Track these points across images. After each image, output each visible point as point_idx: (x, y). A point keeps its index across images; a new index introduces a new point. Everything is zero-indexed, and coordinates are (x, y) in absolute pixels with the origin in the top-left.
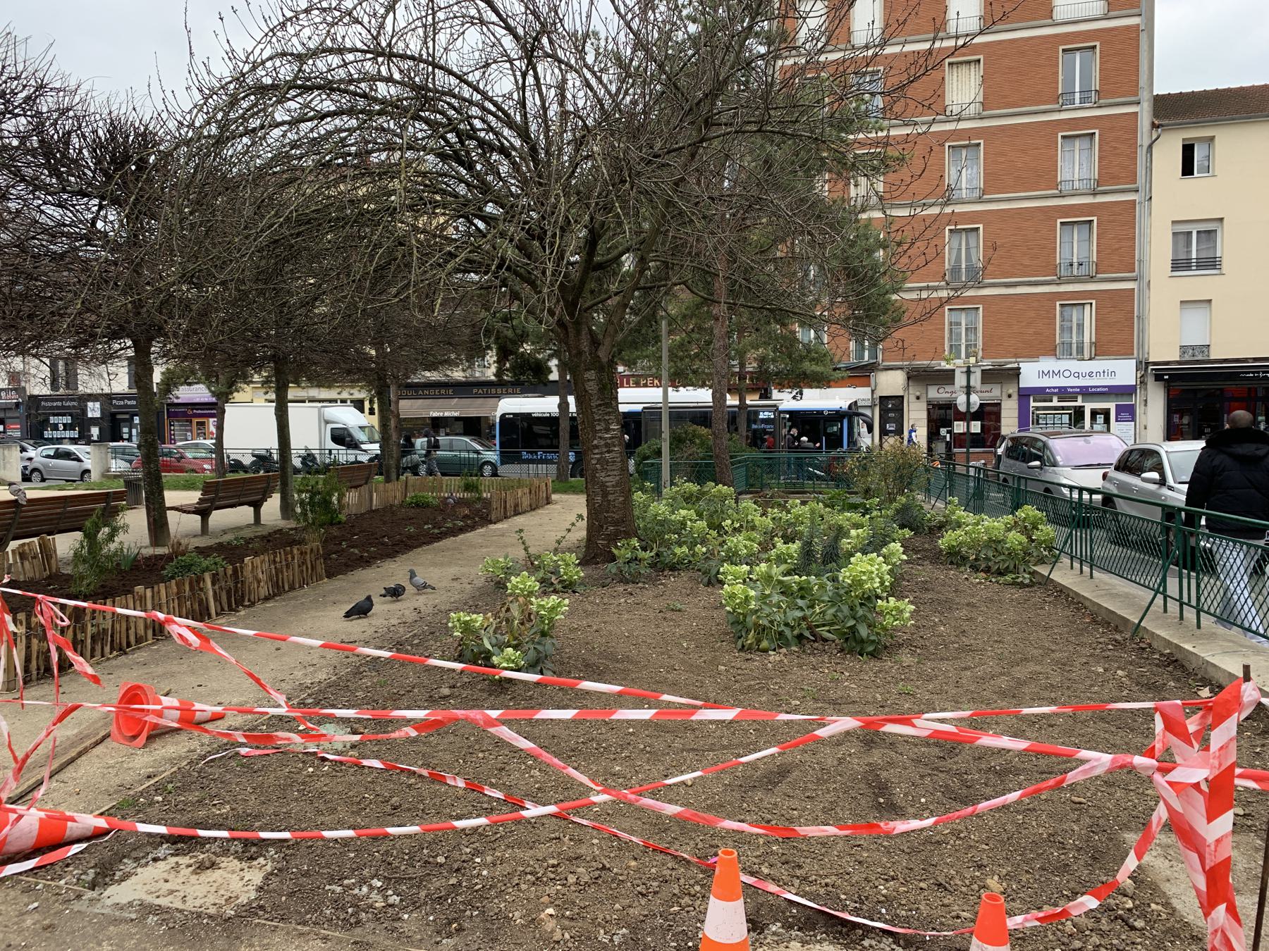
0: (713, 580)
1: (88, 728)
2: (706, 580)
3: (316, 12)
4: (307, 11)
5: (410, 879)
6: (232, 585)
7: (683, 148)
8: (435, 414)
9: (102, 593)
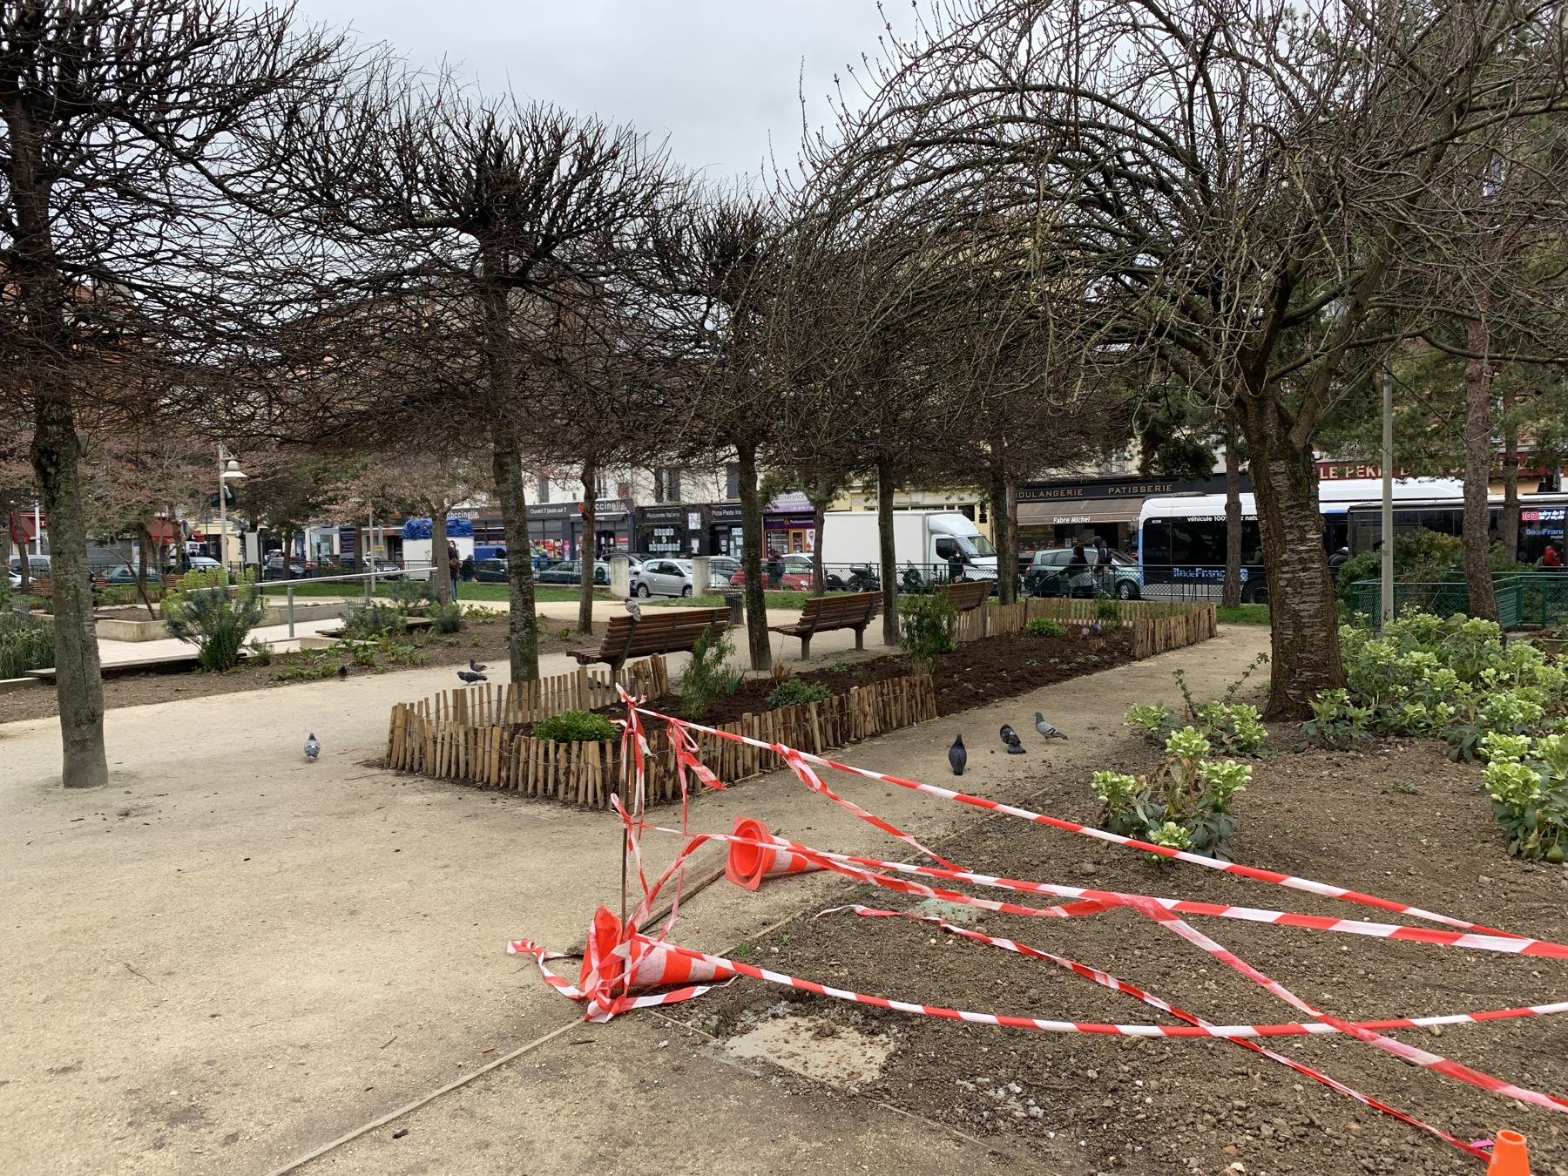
0: (1467, 754)
1: (704, 862)
2: (1455, 752)
3: (938, 54)
4: (929, 55)
5: (1055, 1090)
6: (838, 717)
7: (1424, 149)
8: (1060, 521)
9: (710, 718)
